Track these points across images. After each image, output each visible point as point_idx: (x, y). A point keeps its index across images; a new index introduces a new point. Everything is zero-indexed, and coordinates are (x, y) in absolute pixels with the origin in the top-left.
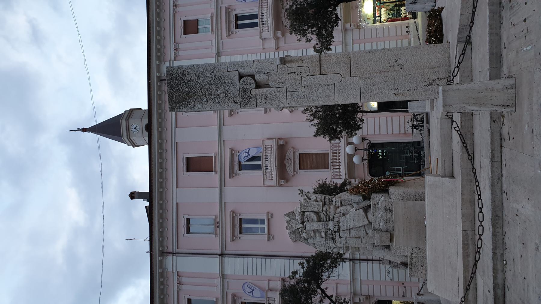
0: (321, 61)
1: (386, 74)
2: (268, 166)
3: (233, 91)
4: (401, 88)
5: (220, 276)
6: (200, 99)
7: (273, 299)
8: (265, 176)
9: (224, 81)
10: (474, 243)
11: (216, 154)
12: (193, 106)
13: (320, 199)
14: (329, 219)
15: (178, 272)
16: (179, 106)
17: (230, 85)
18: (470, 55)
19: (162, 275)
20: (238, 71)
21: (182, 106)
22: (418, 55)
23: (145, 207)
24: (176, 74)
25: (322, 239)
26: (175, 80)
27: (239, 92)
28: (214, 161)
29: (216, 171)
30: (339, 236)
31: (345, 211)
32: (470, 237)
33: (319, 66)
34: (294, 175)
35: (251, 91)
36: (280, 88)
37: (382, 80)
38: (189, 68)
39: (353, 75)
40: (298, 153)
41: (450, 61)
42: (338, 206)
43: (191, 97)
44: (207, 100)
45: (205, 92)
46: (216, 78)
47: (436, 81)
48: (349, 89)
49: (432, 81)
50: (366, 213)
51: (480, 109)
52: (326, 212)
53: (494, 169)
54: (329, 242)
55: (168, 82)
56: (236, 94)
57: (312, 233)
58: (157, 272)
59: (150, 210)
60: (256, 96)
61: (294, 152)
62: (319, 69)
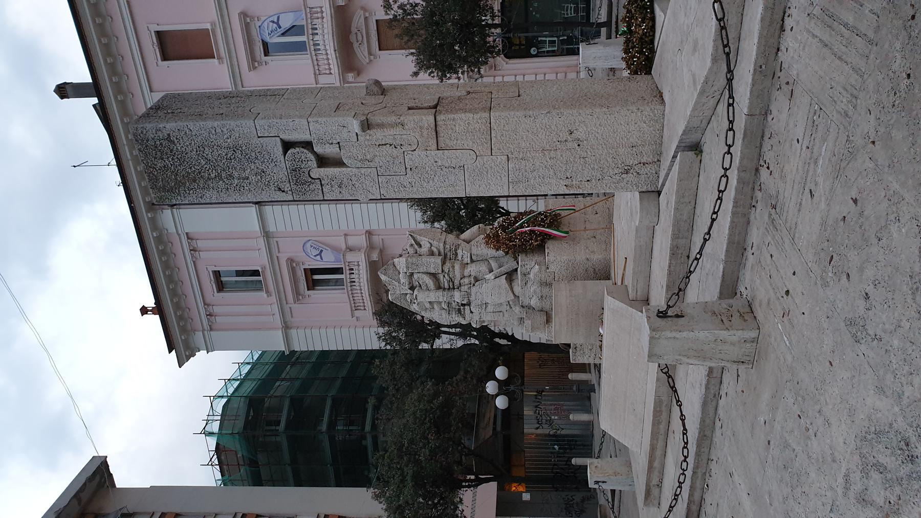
0: (438, 127)
1: (552, 154)
2: (354, 282)
3: (275, 171)
4: (576, 176)
5: (261, 234)
6: (212, 183)
7: (319, 10)
8: (316, 67)
9: (253, 154)
10: (669, 410)
11: (213, 24)
12: (200, 195)
13: (437, 248)
14: (453, 285)
15: (187, 234)
16: (174, 195)
17: (268, 161)
18: (698, 170)
19: (159, 240)
20: (279, 136)
21: (179, 194)
22: (609, 126)
23: (93, 105)
24: (153, 139)
25: (443, 312)
26: (155, 150)
27: (287, 174)
28: (215, 49)
29: (220, 58)
30: (469, 311)
31: (478, 273)
32: (665, 403)
33: (435, 136)
34: (371, 61)
35: (311, 173)
36: (365, 170)
37: (547, 163)
38: (179, 130)
39: (495, 153)
40: (374, 19)
41: (662, 137)
42: (466, 263)
43: (195, 181)
44: (226, 186)
45: (219, 172)
46: (237, 149)
47: (636, 168)
48: (489, 176)
49: (629, 168)
50: (511, 281)
51: (702, 363)
52: (448, 275)
53: (709, 386)
54: (454, 316)
55: (140, 153)
56: (281, 176)
57: (428, 306)
58: (146, 218)
59: (102, 111)
60: (321, 181)
61: (366, 18)
62: (435, 141)
